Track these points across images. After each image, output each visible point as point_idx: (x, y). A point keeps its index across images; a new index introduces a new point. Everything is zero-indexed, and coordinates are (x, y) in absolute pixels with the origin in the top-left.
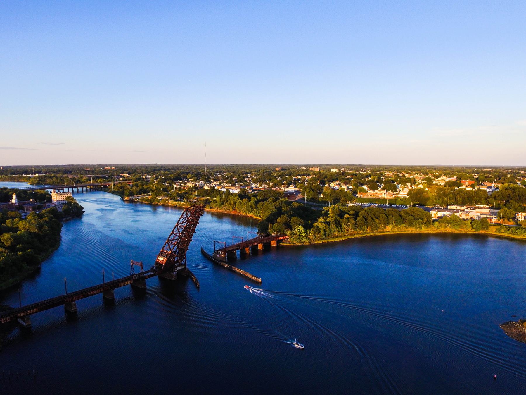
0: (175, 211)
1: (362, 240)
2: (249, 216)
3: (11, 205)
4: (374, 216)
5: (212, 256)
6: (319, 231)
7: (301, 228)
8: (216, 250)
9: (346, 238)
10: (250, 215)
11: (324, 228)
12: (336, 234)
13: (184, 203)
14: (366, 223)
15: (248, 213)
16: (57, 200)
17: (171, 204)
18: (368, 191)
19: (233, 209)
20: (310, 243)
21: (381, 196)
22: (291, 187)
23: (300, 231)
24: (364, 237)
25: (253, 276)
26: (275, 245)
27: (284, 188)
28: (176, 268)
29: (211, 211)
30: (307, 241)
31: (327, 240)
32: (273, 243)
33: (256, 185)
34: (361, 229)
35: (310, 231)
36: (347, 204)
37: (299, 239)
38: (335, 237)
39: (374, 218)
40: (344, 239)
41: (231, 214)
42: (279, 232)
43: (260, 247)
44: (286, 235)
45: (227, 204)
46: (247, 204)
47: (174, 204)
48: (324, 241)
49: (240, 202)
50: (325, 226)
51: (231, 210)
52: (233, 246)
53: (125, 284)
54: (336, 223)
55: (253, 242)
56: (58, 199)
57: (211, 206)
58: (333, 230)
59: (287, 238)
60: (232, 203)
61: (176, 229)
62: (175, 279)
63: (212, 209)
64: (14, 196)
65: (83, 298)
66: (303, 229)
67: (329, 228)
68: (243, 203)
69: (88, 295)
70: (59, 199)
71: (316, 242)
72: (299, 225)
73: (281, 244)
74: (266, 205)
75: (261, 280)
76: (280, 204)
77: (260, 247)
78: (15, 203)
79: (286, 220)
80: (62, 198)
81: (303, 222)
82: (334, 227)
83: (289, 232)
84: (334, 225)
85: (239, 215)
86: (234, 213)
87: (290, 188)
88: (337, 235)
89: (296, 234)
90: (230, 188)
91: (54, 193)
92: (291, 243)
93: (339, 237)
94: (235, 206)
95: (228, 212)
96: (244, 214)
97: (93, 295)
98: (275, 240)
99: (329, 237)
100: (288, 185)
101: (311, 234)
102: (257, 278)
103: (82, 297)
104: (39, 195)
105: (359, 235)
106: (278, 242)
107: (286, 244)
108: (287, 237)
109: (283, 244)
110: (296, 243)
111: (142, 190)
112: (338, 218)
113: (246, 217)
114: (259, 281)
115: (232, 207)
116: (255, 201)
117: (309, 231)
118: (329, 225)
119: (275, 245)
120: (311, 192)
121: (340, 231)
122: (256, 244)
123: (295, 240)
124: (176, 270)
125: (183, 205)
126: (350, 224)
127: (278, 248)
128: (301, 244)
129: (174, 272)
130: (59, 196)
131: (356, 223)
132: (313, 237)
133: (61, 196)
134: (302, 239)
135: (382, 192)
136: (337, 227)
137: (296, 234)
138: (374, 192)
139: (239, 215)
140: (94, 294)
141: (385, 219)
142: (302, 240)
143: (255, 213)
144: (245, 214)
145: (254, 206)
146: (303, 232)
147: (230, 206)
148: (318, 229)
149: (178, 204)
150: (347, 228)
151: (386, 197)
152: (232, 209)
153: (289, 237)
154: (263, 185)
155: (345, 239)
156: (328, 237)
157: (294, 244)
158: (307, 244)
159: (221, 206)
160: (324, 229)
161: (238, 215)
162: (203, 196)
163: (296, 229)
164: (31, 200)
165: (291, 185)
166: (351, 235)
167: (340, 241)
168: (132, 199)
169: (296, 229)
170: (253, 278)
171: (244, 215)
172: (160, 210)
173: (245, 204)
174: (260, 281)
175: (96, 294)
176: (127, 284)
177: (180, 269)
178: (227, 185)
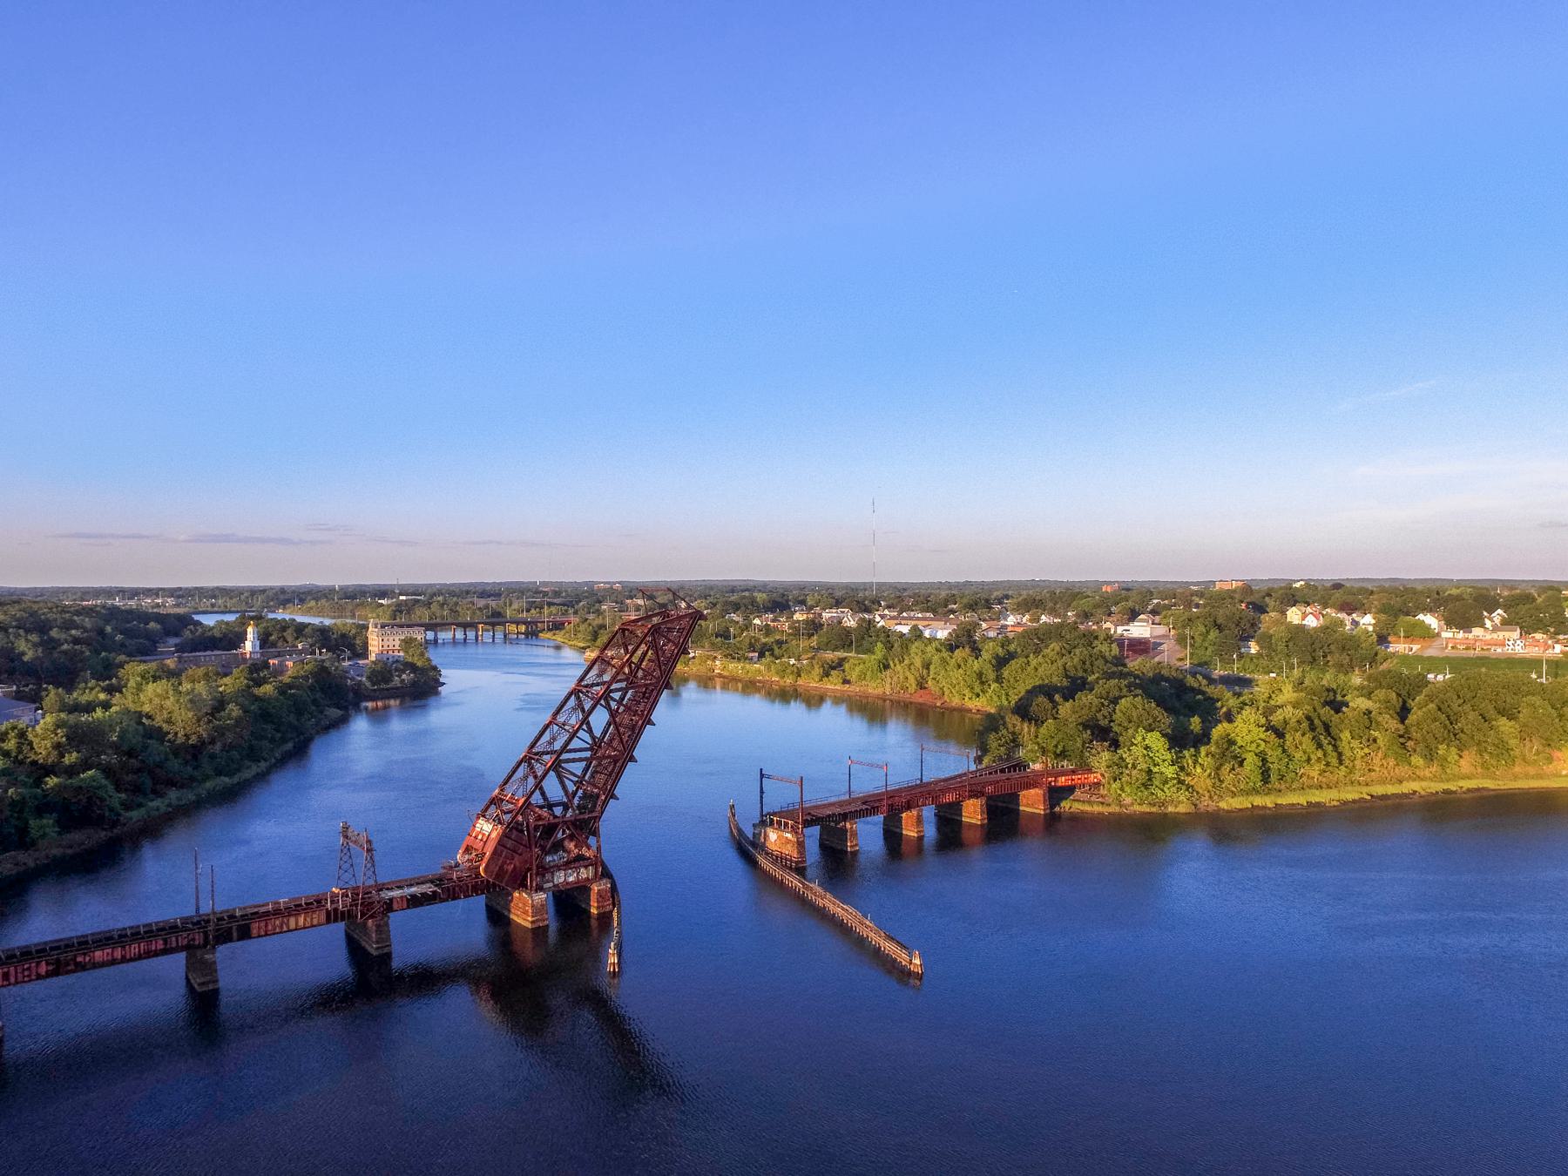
1: (1439, 810)
2: (970, 711)
4: (1491, 707)
6: (1235, 757)
7: (1156, 741)
9: (1362, 793)
11: (1258, 746)
12: (1315, 774)
13: (762, 668)
14: (1453, 735)
17: (723, 670)
18: (1438, 635)
20: (1195, 805)
21: (1499, 650)
22: (1142, 620)
23: (1151, 755)
24: (1446, 792)
25: (891, 938)
26: (1040, 809)
27: (1116, 626)
28: (548, 876)
29: (846, 691)
30: (1183, 796)
31: (1273, 797)
32: (1032, 803)
33: (1019, 617)
34: (1430, 756)
35: (1196, 756)
37: (1146, 786)
38: (1310, 787)
39: (1492, 713)
40: (1350, 797)
42: (1062, 755)
43: (973, 813)
44: (1090, 771)
45: (898, 667)
48: (1259, 801)
49: (943, 660)
50: (1263, 736)
53: (281, 927)
54: (1312, 728)
56: (383, 646)
57: (848, 678)
58: (1298, 755)
59: (1095, 783)
60: (918, 662)
61: (572, 702)
63: (848, 686)
64: (251, 632)
65: (49, 975)
66: (1167, 746)
67: (1280, 746)
69: (77, 964)
71: (1223, 805)
72: (1150, 729)
75: (917, 961)
76: (1084, 663)
77: (973, 813)
79: (1093, 710)
81: (1166, 720)
82: (1307, 743)
83: (1106, 755)
84: (1303, 735)
85: (938, 704)
86: (921, 700)
87: (1136, 624)
88: (1320, 778)
89: (1134, 767)
90: (927, 623)
91: (374, 629)
92: (1109, 805)
93: (1329, 787)
96: (956, 701)
97: (103, 965)
98: (1041, 787)
99: (1283, 787)
100: (1133, 616)
101: (1199, 770)
102: (903, 946)
103: (43, 969)
105: (1424, 784)
106: (1056, 795)
107: (1087, 808)
108: (1092, 778)
109: (1078, 807)
110: (1133, 803)
112: (1326, 712)
115: (916, 679)
116: (997, 657)
117: (1192, 756)
118: (1280, 734)
120: (1213, 634)
121: (1334, 761)
122: (950, 798)
123: (1127, 789)
124: (551, 885)
125: (759, 671)
126: (1376, 734)
127: (1052, 820)
128: (1154, 810)
131: (1407, 730)
132: (1208, 781)
134: (1163, 791)
135: (1504, 633)
136: (1320, 746)
137: (1134, 767)
138: (1466, 635)
140: (113, 962)
141: (1549, 721)
142: (1160, 794)
143: (995, 698)
145: (992, 675)
146: (1164, 761)
147: (908, 674)
148: (1230, 753)
149: (743, 668)
150: (1366, 751)
151: (1521, 651)
152: (914, 686)
153: (1103, 775)
154: (1043, 617)
155: (1356, 797)
156: (1277, 785)
157: (1126, 807)
158: (1182, 809)
159: (879, 674)
160: (1261, 748)
162: (835, 649)
163: (1136, 745)
165: (1142, 616)
166: (1383, 782)
167: (1335, 803)
169: (1133, 744)
173: (959, 666)
174: (915, 964)
175: (124, 960)
176: (292, 925)
177: (571, 879)
178: (920, 615)
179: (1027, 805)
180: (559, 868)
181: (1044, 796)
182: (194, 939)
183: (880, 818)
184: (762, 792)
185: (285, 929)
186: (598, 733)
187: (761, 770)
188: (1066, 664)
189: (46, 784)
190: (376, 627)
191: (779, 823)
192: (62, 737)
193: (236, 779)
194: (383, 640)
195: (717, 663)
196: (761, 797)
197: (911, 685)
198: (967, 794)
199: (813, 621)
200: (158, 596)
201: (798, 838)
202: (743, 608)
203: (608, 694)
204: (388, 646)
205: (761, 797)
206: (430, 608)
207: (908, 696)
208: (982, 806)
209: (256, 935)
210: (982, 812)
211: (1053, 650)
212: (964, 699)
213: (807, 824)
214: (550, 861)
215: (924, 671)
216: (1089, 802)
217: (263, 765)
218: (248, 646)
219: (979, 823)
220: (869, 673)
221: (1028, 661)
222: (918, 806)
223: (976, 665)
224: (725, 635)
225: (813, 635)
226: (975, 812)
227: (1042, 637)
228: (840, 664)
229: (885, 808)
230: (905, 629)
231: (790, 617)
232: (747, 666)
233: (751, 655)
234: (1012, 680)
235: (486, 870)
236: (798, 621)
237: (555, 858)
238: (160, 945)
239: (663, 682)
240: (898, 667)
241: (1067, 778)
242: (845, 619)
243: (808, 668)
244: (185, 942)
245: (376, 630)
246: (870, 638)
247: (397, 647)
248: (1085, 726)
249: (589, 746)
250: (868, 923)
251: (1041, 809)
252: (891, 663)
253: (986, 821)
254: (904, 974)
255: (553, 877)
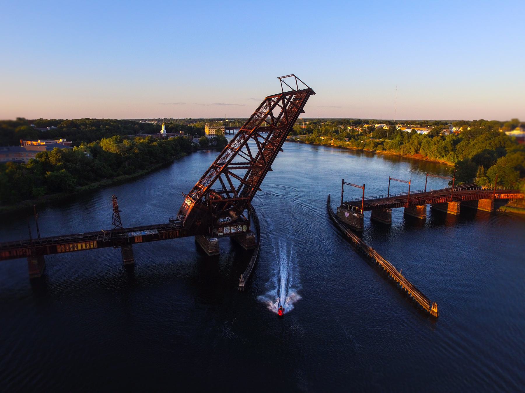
0: (334, 151)
2: (439, 163)
3: (160, 136)
5: (335, 213)
8: (346, 202)
10: (442, 160)
13: (350, 143)
15: (439, 158)
16: (209, 134)
19: (417, 151)
25: (414, 288)
26: (489, 209)
36: (242, 290)
41: (411, 158)
42: (501, 183)
43: (453, 208)
45: (407, 144)
46: (438, 143)
47: (337, 145)
51: (412, 153)
52: (389, 199)
55: (437, 197)
56: (210, 133)
57: (385, 148)
59: (520, 199)
60: (416, 142)
62: (213, 254)
63: (385, 151)
64: (163, 127)
68: (432, 142)
70: (211, 133)
73: (503, 209)
74: (472, 144)
75: (435, 310)
77: (453, 208)
78: (163, 134)
80: (212, 132)
86: (416, 158)
90: (418, 129)
94: (420, 147)
95: (408, 156)
96: (432, 159)
98: (490, 199)
104: (194, 129)
106: (497, 203)
107: (515, 211)
109: (509, 210)
111: (309, 130)
113: (435, 163)
114: (430, 309)
119: (489, 209)
122: (442, 200)
124: (222, 234)
125: (349, 145)
127: (494, 214)
129: (215, 236)
130: (211, 130)
133: (213, 130)
138: (100, 239)
139: (423, 161)
143: (451, 158)
144: (434, 159)
147: (411, 147)
149: (342, 143)
152: (413, 152)
159: (398, 146)
161: (422, 161)
164: (181, 132)
168: (293, 138)
170: (413, 293)
171: (431, 160)
172: (322, 150)
173: (435, 144)
177: (233, 231)
178: (415, 126)
179: (480, 207)
180: (226, 225)
181: (492, 203)
182: (26, 252)
183: (402, 209)
184: (343, 191)
185: (76, 249)
186: (254, 157)
187: (343, 180)
188: (491, 143)
189: (46, 174)
190: (208, 126)
191: (351, 208)
192: (60, 156)
193: (131, 176)
194: (210, 131)
195: (332, 141)
196: (342, 194)
197: (412, 151)
198: (451, 199)
199: (371, 127)
200: (152, 121)
201: (360, 217)
202: (344, 123)
203: (256, 132)
204: (212, 133)
205: (342, 194)
206: (235, 124)
207: (410, 156)
208: (458, 206)
209: (60, 252)
210: (457, 209)
211: (482, 138)
212: (436, 158)
213: (365, 209)
214: (221, 221)
215: (419, 146)
216: (517, 208)
217: (145, 171)
218: (162, 132)
219: (455, 214)
220: (394, 146)
221: (469, 142)
222: (425, 204)
223: (443, 143)
224: (336, 132)
225: (371, 132)
226: (453, 209)
227: (472, 134)
228: (382, 143)
229: (407, 204)
230: (409, 131)
231: (362, 127)
232: (344, 142)
233: (345, 139)
234: (460, 150)
235: (184, 224)
236: (365, 127)
237: (225, 220)
238: (7, 254)
239: (288, 128)
240: (407, 144)
241: (505, 195)
242: (384, 127)
243: (369, 144)
244: (21, 253)
245: (208, 127)
246: (394, 134)
247: (215, 133)
248: (516, 168)
249: (249, 162)
250: (400, 275)
251: (489, 210)
252: (404, 142)
253: (459, 214)
254: (426, 314)
255: (223, 230)
